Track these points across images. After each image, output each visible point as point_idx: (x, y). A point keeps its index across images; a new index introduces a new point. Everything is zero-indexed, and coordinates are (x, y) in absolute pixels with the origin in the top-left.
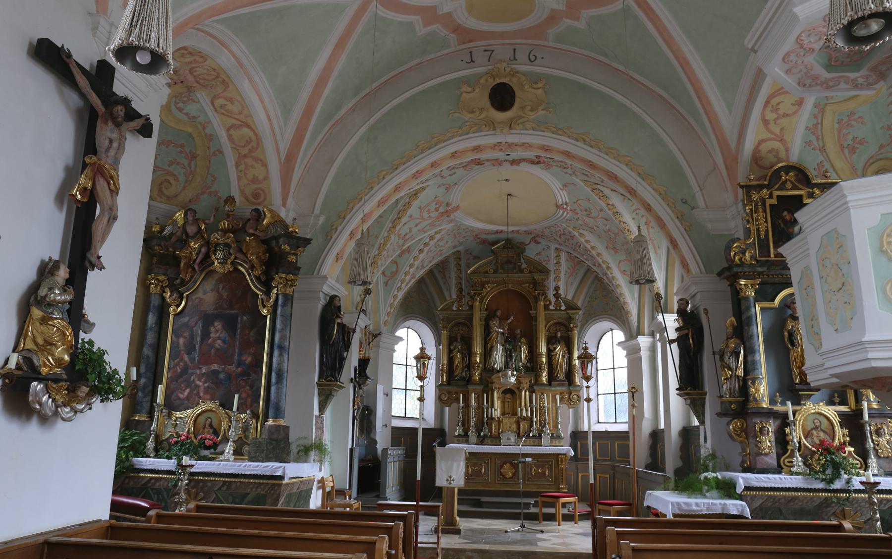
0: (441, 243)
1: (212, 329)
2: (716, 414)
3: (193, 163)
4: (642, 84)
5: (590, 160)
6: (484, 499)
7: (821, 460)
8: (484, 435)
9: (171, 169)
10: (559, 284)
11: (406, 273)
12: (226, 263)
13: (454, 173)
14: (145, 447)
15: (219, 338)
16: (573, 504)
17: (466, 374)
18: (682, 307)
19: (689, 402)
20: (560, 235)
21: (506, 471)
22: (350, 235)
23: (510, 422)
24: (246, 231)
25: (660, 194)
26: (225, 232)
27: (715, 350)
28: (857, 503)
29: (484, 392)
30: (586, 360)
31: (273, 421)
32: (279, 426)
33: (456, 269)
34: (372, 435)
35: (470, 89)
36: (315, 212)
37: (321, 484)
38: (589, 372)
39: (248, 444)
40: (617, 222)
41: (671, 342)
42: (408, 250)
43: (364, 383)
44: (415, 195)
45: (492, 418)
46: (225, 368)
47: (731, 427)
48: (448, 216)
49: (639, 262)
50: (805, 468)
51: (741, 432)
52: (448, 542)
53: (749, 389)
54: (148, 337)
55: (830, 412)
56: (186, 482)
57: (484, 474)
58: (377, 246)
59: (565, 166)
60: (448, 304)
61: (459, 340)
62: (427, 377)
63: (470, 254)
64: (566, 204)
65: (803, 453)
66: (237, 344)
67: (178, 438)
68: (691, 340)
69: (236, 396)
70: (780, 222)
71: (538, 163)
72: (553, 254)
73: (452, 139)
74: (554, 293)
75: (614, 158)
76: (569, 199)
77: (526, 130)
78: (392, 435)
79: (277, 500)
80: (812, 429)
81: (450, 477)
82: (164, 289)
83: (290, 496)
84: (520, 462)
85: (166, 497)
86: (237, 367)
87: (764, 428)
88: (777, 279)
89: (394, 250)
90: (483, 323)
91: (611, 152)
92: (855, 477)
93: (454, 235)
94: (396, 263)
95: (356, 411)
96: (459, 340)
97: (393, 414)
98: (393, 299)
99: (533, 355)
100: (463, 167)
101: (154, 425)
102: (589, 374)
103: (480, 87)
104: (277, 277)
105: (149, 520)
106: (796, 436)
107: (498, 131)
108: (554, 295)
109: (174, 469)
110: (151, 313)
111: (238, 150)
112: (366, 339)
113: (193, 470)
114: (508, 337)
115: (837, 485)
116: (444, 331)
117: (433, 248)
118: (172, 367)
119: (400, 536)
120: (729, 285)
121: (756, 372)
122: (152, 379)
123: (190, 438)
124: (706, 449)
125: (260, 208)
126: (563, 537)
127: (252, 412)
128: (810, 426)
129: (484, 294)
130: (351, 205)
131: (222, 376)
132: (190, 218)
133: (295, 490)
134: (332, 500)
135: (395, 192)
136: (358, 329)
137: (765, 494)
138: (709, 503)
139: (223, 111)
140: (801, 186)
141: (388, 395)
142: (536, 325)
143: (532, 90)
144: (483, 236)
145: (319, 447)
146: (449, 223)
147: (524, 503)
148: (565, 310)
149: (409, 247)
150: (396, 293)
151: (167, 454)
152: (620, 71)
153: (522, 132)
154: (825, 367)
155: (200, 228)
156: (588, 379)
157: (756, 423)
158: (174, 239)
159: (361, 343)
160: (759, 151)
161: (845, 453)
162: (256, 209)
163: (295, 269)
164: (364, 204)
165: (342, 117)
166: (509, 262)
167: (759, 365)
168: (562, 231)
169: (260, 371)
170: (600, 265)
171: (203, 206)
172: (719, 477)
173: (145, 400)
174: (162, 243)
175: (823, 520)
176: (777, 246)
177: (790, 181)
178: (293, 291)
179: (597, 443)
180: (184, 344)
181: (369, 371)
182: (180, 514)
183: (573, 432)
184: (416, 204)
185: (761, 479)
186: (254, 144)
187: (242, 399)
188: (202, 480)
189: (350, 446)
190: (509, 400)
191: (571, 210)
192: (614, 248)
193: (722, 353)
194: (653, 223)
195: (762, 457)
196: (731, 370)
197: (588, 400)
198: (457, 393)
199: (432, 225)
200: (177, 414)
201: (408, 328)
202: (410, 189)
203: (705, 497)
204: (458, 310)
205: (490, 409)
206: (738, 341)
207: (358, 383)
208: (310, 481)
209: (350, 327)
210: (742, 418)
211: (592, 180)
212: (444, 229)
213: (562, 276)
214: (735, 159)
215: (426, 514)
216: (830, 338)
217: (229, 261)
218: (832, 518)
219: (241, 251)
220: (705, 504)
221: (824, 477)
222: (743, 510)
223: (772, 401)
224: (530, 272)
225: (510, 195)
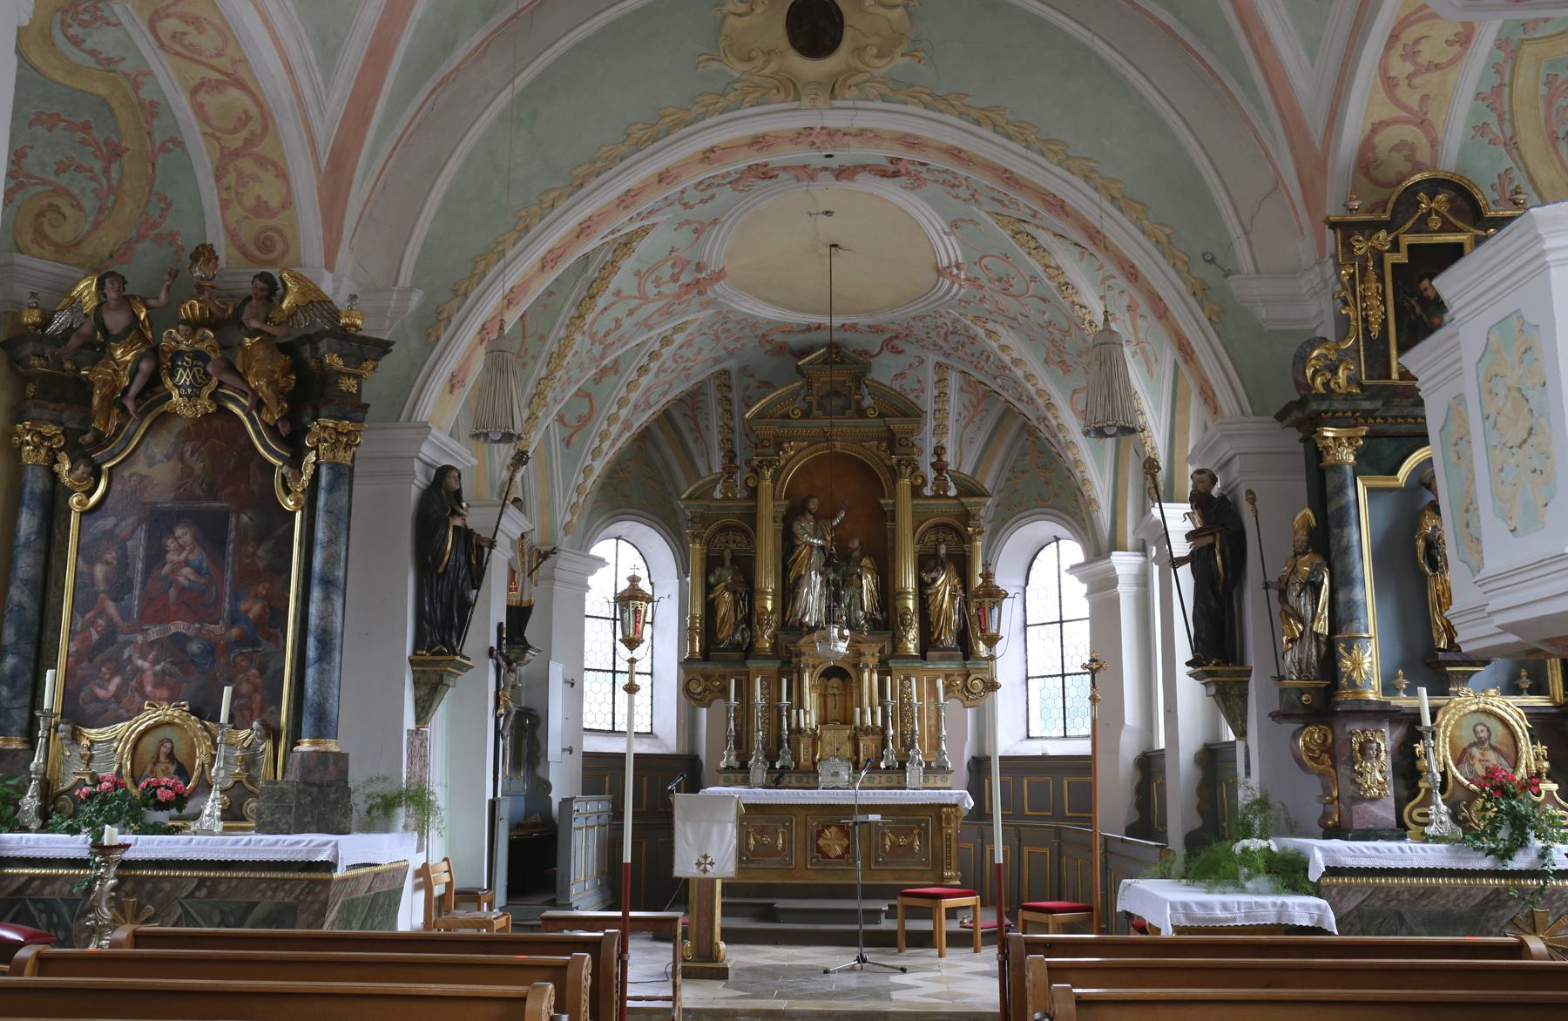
0: (688, 353)
1: (170, 544)
2: (1270, 715)
3: (114, 168)
5: (1005, 165)
7: (1488, 810)
9: (64, 180)
10: (944, 441)
11: (612, 419)
12: (198, 396)
13: (712, 197)
14: (17, 808)
15: (187, 563)
18: (1201, 488)
19: (1213, 690)
20: (946, 334)
21: (830, 842)
22: (479, 333)
23: (836, 737)
24: (242, 324)
25: (1157, 242)
26: (194, 325)
27: (1269, 579)
28: (1560, 899)
29: (781, 673)
30: (987, 600)
31: (313, 744)
32: (325, 754)
33: (720, 410)
34: (540, 772)
35: (743, 8)
36: (401, 282)
37: (421, 879)
38: (995, 627)
39: (257, 797)
40: (1066, 303)
42: (615, 367)
43: (520, 659)
44: (625, 245)
45: (799, 730)
46: (200, 629)
47: (1301, 742)
48: (700, 293)
50: (1454, 826)
51: (1322, 752)
52: (694, 995)
53: (1340, 660)
54: (20, 563)
55: (1509, 710)
56: (112, 882)
57: (783, 849)
58: (544, 357)
59: (954, 182)
60: (703, 485)
61: (728, 563)
62: (643, 641)
63: (752, 376)
64: (958, 266)
65: (1451, 796)
66: (229, 575)
67: (94, 786)
68: (1218, 558)
69: (227, 691)
70: (1414, 303)
71: (896, 174)
72: (931, 376)
73: (704, 119)
74: (934, 460)
75: (1059, 164)
76: (964, 254)
77: (867, 99)
79: (321, 915)
80: (1471, 745)
81: (706, 857)
82: (55, 455)
83: (349, 906)
85: (67, 917)
86: (229, 628)
87: (1368, 745)
88: (1403, 427)
89: (582, 368)
90: (780, 525)
91: (1052, 150)
92: (1558, 845)
94: (589, 396)
95: (502, 719)
96: (728, 563)
97: (586, 725)
98: (582, 475)
99: (887, 593)
100: (730, 183)
101: (38, 759)
104: (315, 427)
105: (18, 969)
106: (1437, 760)
107: (805, 102)
108: (933, 465)
109: (85, 854)
110: (25, 510)
111: (218, 139)
112: (523, 563)
113: (128, 855)
115: (1520, 862)
117: (669, 363)
118: (79, 627)
119: (584, 984)
120: (1300, 441)
121: (1355, 625)
122: (33, 656)
123: (123, 785)
124: (1248, 788)
125: (275, 272)
127: (264, 724)
128: (1467, 737)
129: (782, 463)
130: (481, 267)
131: (194, 647)
132: (112, 295)
133: (362, 892)
134: (448, 912)
135: (578, 237)
137: (1368, 883)
138: (1250, 903)
139: (178, 48)
140: (1460, 224)
142: (894, 531)
143: (881, 10)
144: (779, 338)
145: (418, 799)
146: (704, 309)
147: (866, 912)
148: (956, 497)
149: (616, 361)
150: (588, 461)
151: (69, 822)
154: (1488, 609)
155: (137, 317)
157: (1352, 734)
158: (74, 342)
159: (512, 572)
160: (1374, 147)
161: (1538, 794)
162: (263, 274)
163: (355, 409)
167: (1361, 610)
168: (949, 324)
169: (281, 635)
170: (1031, 400)
171: (142, 268)
172: (1274, 848)
173: (15, 704)
174: (48, 352)
175: (1489, 934)
176: (1403, 348)
177: (1437, 213)
178: (353, 460)
179: (1026, 781)
180: (107, 578)
181: (530, 633)
182: (100, 954)
183: (973, 758)
184: (627, 265)
185: (1361, 851)
186: (256, 125)
187: (242, 697)
188: (152, 877)
189: (489, 795)
190: (835, 691)
191: (968, 279)
192: (1062, 362)
193: (1283, 585)
194: (1144, 308)
195: (1366, 804)
196: (1302, 622)
198: (724, 678)
199: (666, 313)
200: (92, 733)
201: (618, 538)
202: (613, 232)
203: (1243, 890)
204: (726, 498)
205: (794, 712)
206: (1318, 560)
208: (398, 872)
210: (1324, 724)
211: (1013, 212)
213: (951, 423)
214: (1322, 165)
216: (1501, 551)
217: (206, 392)
218: (1507, 930)
219: (231, 368)
220: (1243, 906)
221: (1493, 846)
222: (1321, 917)
223: (1389, 688)
224: (881, 415)
225: (835, 246)
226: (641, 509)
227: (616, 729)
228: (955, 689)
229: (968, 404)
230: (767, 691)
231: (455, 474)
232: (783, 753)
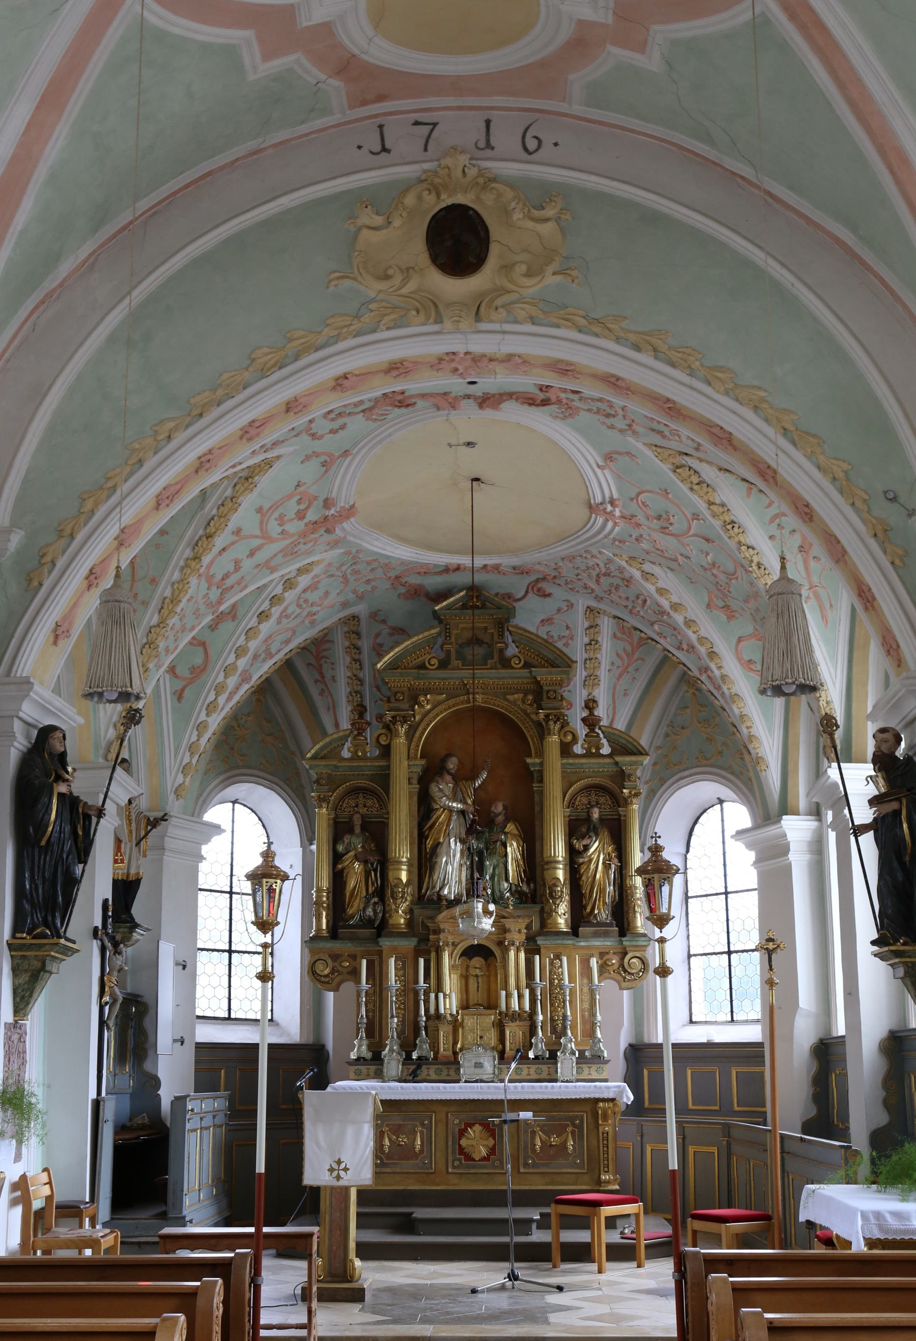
4: (795, 211)
8: (419, 1058)
10: (595, 693)
11: (228, 670)
13: (343, 427)
16: (633, 1220)
17: (375, 911)
18: (885, 748)
19: (901, 971)
20: (598, 575)
22: (87, 578)
25: (834, 479)
29: (418, 953)
30: (656, 876)
33: (348, 659)
34: (148, 1066)
35: (379, 220)
37: (19, 1193)
40: (732, 544)
41: (858, 831)
42: (232, 613)
43: (126, 939)
44: (247, 479)
45: (438, 1016)
48: (328, 531)
49: (783, 645)
57: (422, 1151)
58: (155, 603)
59: (609, 411)
60: (330, 743)
61: (357, 830)
62: (278, 923)
63: (384, 622)
64: (612, 502)
68: (905, 826)
71: (545, 403)
72: (580, 622)
73: (336, 343)
75: (726, 393)
76: (620, 491)
77: (516, 322)
78: (196, 1062)
81: (339, 1162)
84: (505, 1122)
89: (197, 614)
93: (344, 576)
94: (203, 644)
95: (107, 1008)
96: (357, 830)
97: (199, 1013)
98: (195, 733)
100: (363, 411)
102: (664, 910)
103: (405, 214)
107: (448, 325)
108: (584, 720)
112: (131, 832)
114: (473, 821)
119: (216, 1313)
126: (611, 1300)
129: (418, 718)
130: (89, 505)
134: (48, 1230)
135: (197, 472)
136: (110, 807)
141: (185, 966)
142: (541, 793)
143: (530, 224)
144: (414, 580)
147: (516, 1221)
148: (610, 756)
149: (234, 606)
150: (203, 717)
152: (742, 177)
153: (507, 327)
156: (661, 921)
159: (118, 841)
164: (120, 503)
165: (61, 285)
166: (475, 641)
168: (602, 565)
181: (137, 910)
183: (630, 1045)
184: (249, 502)
189: (93, 1094)
190: (478, 972)
191: (623, 517)
192: (726, 607)
194: (817, 549)
197: (664, 971)
199: (290, 553)
201: (234, 802)
202: (234, 466)
205: (432, 995)
207: (112, 939)
209: (90, 803)
211: (674, 445)
213: (603, 674)
215: (281, 1255)
224: (527, 665)
225: (477, 480)
226: (260, 770)
227: (233, 1016)
229: (621, 652)
230: (402, 972)
231: (59, 735)
232: (420, 1042)
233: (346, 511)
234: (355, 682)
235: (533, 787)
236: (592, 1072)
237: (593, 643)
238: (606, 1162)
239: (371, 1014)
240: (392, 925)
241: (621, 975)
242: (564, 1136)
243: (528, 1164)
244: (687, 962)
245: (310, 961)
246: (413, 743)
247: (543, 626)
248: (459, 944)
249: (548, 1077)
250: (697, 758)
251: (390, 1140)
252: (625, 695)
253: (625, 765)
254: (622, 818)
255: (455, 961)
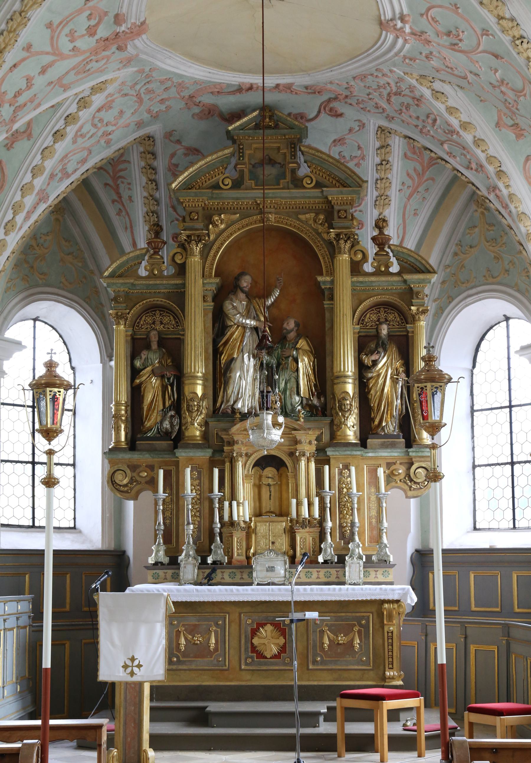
6: (213, 707)
8: (214, 563)
10: (386, 213)
11: (25, 189)
16: (414, 713)
20: (389, 94)
29: (213, 463)
33: (144, 180)
38: (438, 413)
45: (232, 523)
48: (119, 48)
57: (216, 649)
60: (127, 261)
61: (154, 346)
62: (61, 431)
63: (178, 142)
64: (402, 18)
81: (133, 659)
90: (210, 305)
93: (139, 96)
96: (154, 346)
108: (374, 239)
116: (118, 324)
117: (88, 127)
129: (212, 237)
142: (332, 310)
144: (207, 99)
148: (399, 274)
149: (29, 124)
168: (393, 84)
183: (417, 551)
190: (270, 481)
191: (413, 34)
192: (516, 125)
198: (151, 468)
201: (35, 320)
204: (151, 276)
205: (226, 504)
212: (116, 79)
213: (394, 193)
226: (59, 288)
228: (397, 479)
230: (197, 482)
232: (215, 547)
233: (138, 28)
234: (152, 202)
235: (323, 304)
236: (378, 576)
237: (384, 163)
238: (390, 660)
239: (168, 521)
240: (188, 437)
241: (407, 484)
242: (351, 635)
243: (317, 662)
244: (472, 472)
245: (109, 472)
246: (208, 262)
247: (335, 146)
248: (252, 455)
249: (336, 580)
250: (485, 276)
251: (186, 639)
252: (415, 214)
253: (414, 283)
254: (410, 335)
255: (248, 471)
